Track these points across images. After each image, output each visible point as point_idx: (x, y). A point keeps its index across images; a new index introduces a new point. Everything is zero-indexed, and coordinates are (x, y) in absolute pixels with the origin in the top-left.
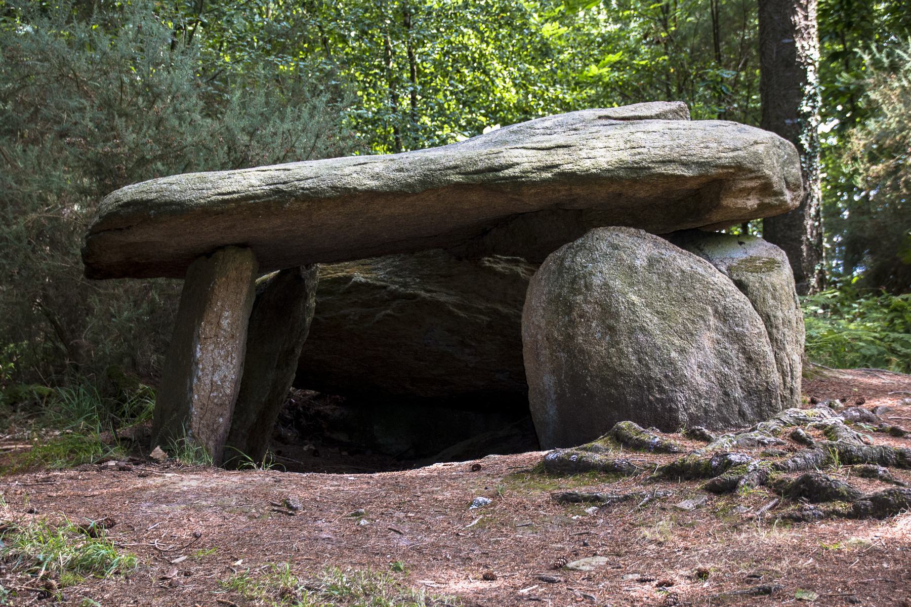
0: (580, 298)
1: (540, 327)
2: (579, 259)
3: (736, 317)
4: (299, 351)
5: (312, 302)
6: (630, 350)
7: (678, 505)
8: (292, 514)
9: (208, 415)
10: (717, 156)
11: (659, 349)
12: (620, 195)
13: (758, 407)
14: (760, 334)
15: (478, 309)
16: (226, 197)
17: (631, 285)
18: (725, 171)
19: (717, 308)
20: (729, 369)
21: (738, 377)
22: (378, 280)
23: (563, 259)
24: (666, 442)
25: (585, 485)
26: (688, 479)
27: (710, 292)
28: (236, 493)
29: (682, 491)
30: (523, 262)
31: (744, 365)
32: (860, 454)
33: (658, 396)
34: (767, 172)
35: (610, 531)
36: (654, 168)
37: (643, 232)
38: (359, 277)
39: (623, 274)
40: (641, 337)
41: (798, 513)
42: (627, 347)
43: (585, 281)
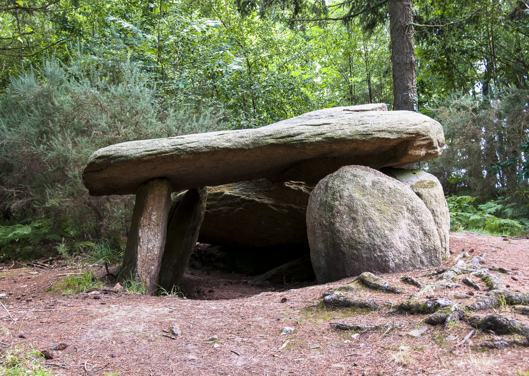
0: (337, 203)
1: (316, 218)
2: (336, 182)
3: (418, 212)
4: (199, 228)
5: (205, 205)
6: (364, 230)
7: (410, 333)
8: (174, 339)
9: (146, 265)
10: (406, 128)
11: (379, 229)
12: (356, 149)
13: (430, 258)
14: (430, 220)
15: (282, 206)
16: (150, 153)
17: (364, 195)
18: (411, 136)
19: (408, 207)
20: (415, 239)
21: (420, 243)
22: (236, 193)
23: (328, 182)
24: (393, 286)
25: (349, 316)
26: (412, 314)
27: (404, 199)
28: (144, 322)
29: (410, 323)
30: (303, 184)
31: (422, 237)
32: (517, 298)
33: (379, 254)
34: (432, 137)
35: (369, 353)
36: (374, 134)
37: (368, 168)
38: (227, 192)
39: (359, 190)
40: (369, 223)
41: (491, 343)
42: (362, 228)
43: (340, 195)
